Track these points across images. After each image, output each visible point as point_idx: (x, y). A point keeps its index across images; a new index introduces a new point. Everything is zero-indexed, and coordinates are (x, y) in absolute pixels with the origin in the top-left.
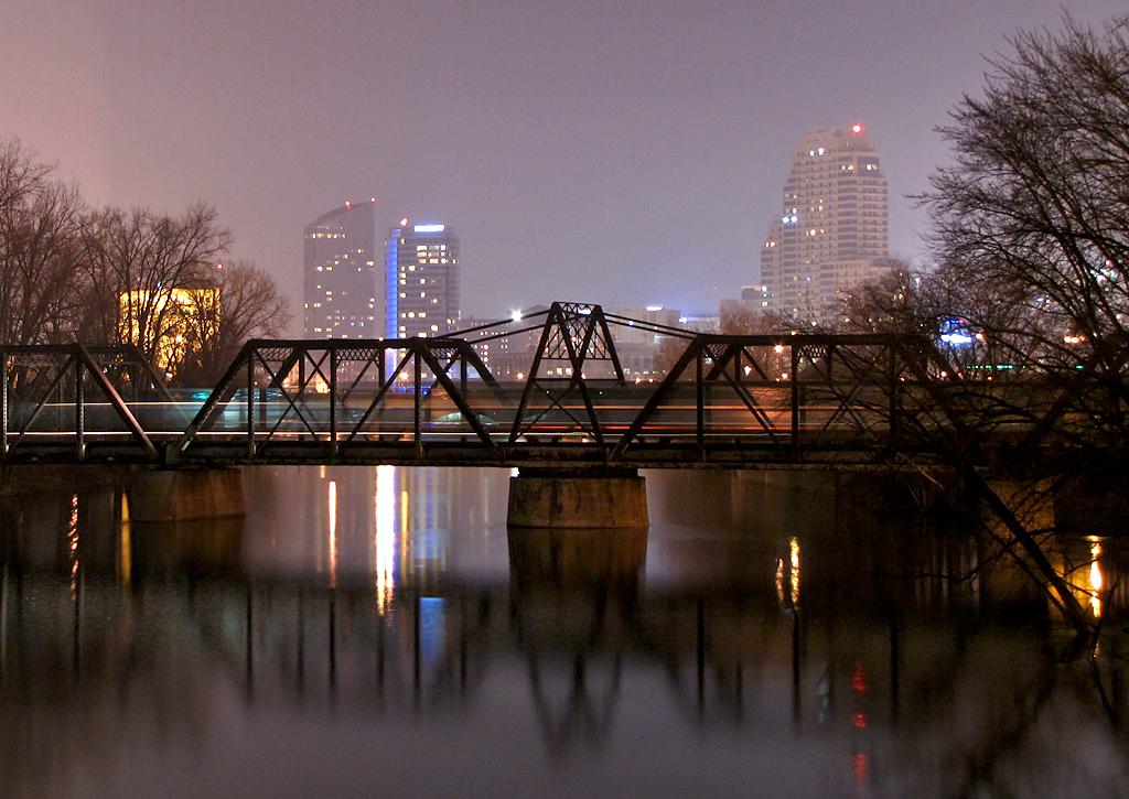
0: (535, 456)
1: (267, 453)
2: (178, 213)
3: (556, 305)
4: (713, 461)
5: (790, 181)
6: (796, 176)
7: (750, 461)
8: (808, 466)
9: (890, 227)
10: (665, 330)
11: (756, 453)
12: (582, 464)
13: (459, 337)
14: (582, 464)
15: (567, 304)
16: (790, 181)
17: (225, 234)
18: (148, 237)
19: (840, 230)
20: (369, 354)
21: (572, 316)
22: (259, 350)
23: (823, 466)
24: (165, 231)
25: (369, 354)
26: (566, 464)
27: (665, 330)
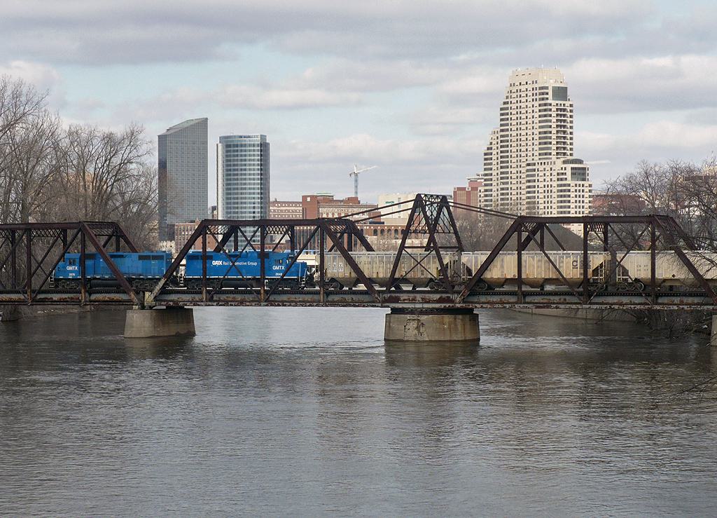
0: (404, 300)
1: (215, 298)
2: (119, 130)
3: (419, 196)
4: (528, 303)
5: (505, 103)
6: (509, 100)
7: (554, 303)
8: (595, 307)
9: (574, 136)
10: (465, 207)
11: (506, 288)
12: (437, 306)
13: (348, 218)
14: (437, 306)
15: (426, 195)
16: (505, 103)
17: (150, 142)
18: (97, 147)
19: (540, 138)
20: (284, 230)
21: (428, 203)
22: (210, 227)
23: (605, 306)
24: (109, 139)
25: (284, 230)
26: (426, 306)
27: (465, 207)
